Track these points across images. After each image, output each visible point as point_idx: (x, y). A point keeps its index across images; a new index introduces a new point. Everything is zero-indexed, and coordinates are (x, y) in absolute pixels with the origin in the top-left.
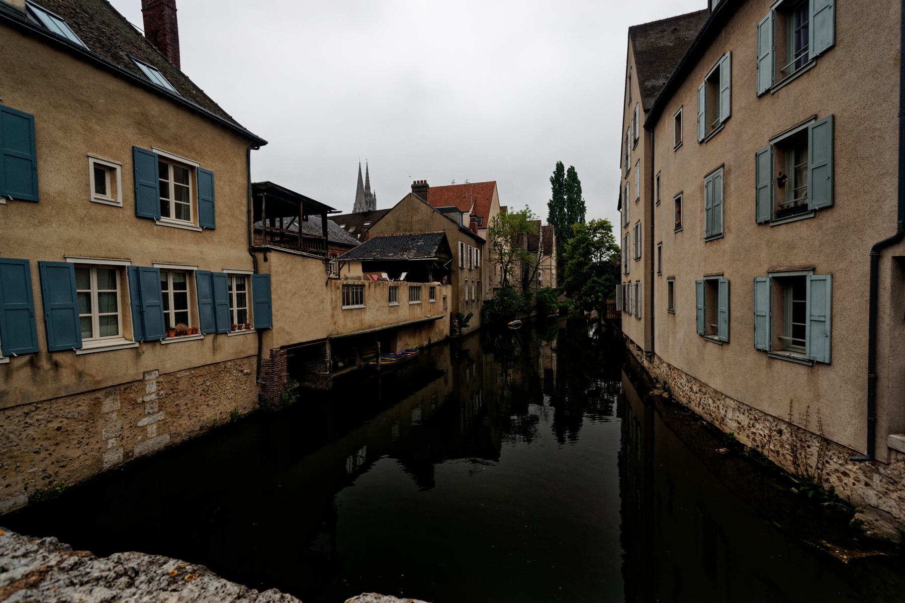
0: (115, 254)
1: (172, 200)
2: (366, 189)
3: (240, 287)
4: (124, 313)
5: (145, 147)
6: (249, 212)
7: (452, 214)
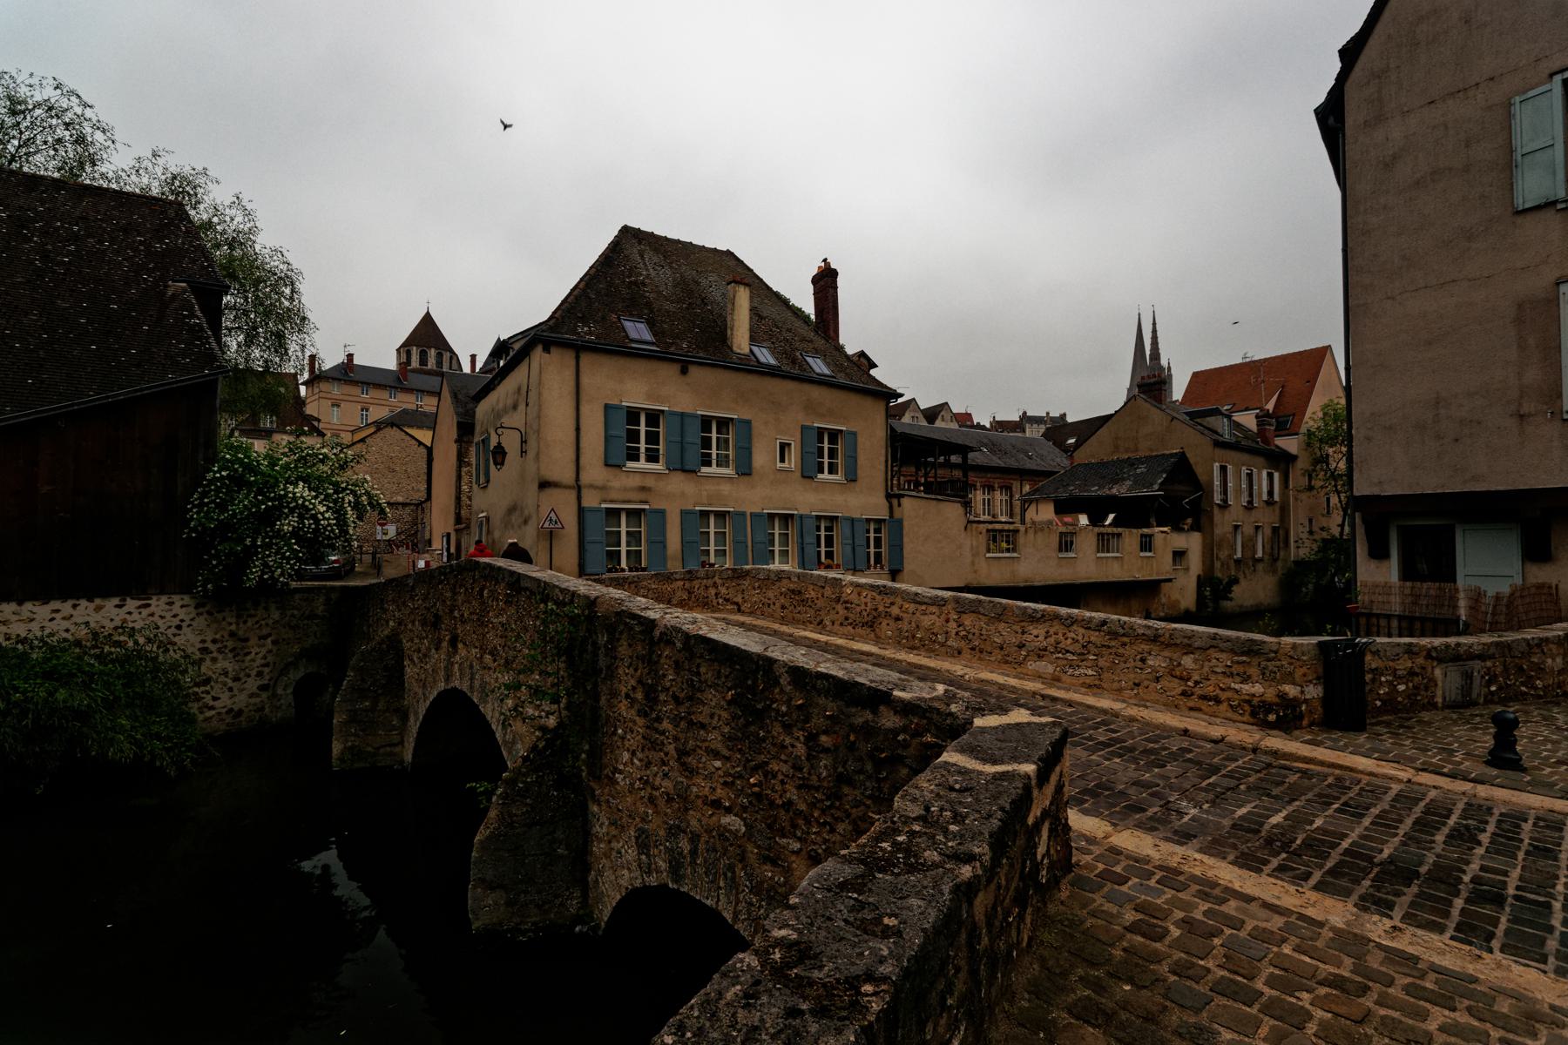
0: (788, 506)
1: (826, 460)
2: (1151, 359)
3: (877, 531)
4: (793, 548)
5: (809, 424)
6: (887, 461)
7: (1210, 419)
